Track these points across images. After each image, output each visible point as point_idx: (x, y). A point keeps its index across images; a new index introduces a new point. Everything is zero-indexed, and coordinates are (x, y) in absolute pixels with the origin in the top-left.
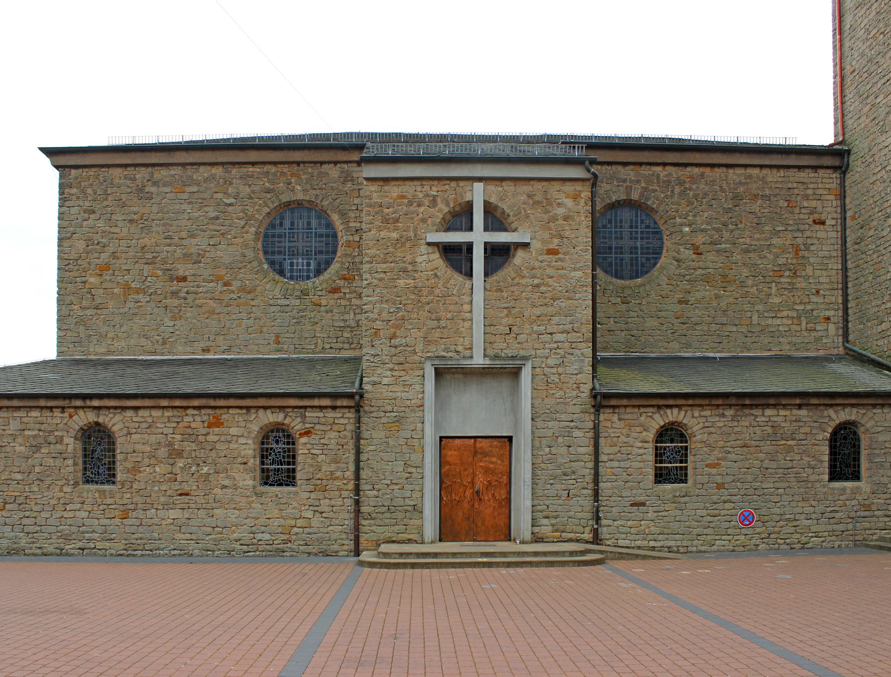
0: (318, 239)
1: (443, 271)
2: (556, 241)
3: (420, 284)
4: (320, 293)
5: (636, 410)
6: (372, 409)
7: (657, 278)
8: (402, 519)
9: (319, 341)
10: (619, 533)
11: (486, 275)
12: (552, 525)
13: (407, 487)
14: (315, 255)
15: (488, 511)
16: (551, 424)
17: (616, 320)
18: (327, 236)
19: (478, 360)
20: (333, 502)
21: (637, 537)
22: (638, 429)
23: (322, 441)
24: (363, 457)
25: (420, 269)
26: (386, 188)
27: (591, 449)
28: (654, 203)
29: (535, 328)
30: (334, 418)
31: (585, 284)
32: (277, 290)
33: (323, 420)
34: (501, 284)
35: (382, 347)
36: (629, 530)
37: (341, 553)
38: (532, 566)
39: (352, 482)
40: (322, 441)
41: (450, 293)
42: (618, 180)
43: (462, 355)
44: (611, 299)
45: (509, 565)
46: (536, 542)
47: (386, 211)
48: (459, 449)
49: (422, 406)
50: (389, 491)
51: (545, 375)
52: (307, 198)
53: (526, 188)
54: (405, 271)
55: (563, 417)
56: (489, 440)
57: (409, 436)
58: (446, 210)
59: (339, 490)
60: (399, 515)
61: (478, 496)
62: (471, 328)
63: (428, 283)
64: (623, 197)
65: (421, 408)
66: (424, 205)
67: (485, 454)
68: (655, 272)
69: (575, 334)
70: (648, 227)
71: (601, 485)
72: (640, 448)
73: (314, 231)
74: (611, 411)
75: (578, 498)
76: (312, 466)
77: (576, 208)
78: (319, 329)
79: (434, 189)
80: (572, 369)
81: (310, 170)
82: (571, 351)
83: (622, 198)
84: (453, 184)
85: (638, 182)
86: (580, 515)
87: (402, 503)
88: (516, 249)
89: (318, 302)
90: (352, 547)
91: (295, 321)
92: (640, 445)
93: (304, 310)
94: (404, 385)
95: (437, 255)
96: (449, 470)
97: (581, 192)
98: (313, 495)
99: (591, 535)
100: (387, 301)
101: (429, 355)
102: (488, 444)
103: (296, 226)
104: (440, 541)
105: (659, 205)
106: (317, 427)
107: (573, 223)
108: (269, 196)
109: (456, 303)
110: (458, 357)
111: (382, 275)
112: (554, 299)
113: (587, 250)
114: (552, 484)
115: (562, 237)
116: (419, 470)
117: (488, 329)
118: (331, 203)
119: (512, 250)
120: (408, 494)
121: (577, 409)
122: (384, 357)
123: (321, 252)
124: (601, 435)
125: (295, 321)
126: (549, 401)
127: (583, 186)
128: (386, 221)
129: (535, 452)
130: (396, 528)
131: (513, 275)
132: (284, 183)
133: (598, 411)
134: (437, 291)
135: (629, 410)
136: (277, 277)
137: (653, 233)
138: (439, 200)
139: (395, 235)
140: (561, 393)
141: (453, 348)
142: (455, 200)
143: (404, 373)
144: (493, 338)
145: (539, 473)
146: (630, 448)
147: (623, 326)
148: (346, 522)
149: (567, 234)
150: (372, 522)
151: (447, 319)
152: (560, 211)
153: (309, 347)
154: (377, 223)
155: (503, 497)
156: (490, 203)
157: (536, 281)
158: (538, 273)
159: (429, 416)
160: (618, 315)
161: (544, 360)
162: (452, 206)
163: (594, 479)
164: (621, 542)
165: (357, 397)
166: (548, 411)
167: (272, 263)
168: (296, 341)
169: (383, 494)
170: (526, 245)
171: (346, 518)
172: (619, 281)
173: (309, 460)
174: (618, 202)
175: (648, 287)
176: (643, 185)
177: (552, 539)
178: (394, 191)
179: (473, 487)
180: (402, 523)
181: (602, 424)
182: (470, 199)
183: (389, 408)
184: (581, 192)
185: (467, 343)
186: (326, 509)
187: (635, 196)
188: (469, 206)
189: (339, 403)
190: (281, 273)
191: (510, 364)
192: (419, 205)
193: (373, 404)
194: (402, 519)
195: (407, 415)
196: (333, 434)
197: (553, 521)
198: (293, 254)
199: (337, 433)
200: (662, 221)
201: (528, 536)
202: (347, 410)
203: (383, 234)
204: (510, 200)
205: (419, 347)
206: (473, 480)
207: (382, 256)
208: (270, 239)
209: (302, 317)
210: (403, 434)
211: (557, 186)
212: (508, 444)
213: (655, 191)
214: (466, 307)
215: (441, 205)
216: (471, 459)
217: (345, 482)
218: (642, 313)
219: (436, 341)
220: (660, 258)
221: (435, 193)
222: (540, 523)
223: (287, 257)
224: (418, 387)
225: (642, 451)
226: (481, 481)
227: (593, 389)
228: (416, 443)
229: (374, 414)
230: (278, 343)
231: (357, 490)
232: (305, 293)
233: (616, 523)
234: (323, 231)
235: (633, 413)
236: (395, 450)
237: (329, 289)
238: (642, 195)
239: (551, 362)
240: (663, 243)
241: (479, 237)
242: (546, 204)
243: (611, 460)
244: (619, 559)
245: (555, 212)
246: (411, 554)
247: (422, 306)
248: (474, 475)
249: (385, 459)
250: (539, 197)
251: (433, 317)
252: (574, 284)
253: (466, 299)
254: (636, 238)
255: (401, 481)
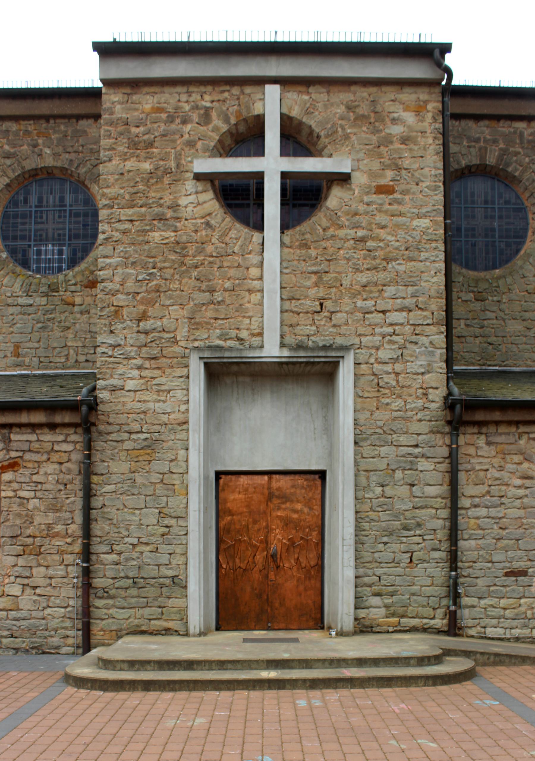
0: (73, 219)
1: (219, 218)
2: (390, 174)
3: (184, 238)
4: (73, 288)
5: (513, 429)
6: (110, 428)
7: (521, 267)
8: (155, 598)
9: (72, 352)
10: (488, 617)
11: (285, 227)
12: (387, 606)
13: (163, 548)
14: (70, 239)
15: (290, 585)
16: (384, 450)
17: (468, 322)
18: (86, 215)
19: (272, 350)
20: (51, 572)
21: (515, 623)
22: (517, 458)
23: (35, 478)
24: (96, 502)
25: (184, 215)
26: (135, 97)
27: (445, 489)
28: (516, 170)
29: (359, 303)
30: (53, 443)
31: (434, 237)
32: (17, 285)
33: (36, 445)
34: (308, 236)
35: (126, 334)
36: (502, 612)
37: (64, 650)
38: (353, 686)
39: (80, 541)
40: (35, 478)
41: (230, 251)
42: (469, 139)
43: (247, 344)
44: (461, 294)
45: (314, 684)
46: (362, 632)
47: (134, 130)
48: (246, 490)
49: (186, 423)
50: (135, 555)
51: (374, 374)
52: (59, 164)
53: (344, 96)
54: (161, 218)
55: (403, 439)
56: (292, 477)
57: (166, 470)
58: (224, 128)
59: (60, 552)
60: (151, 592)
61: (275, 561)
62: (261, 304)
63: (196, 237)
64: (476, 161)
65: (184, 427)
66: (191, 121)
67: (285, 498)
68: (518, 261)
69: (420, 312)
70: (507, 202)
71: (461, 543)
72: (519, 487)
73: (68, 208)
74: (475, 430)
75: (425, 565)
76: (19, 515)
77: (421, 126)
78: (71, 336)
79: (207, 97)
80: (415, 366)
81: (62, 127)
82: (414, 338)
83: (474, 162)
84: (236, 90)
85: (495, 141)
86: (428, 591)
87: (155, 573)
88: (329, 188)
89: (70, 300)
90: (80, 640)
91: (40, 325)
92: (519, 482)
93: (52, 311)
94: (158, 391)
95: (210, 195)
96: (230, 523)
97: (426, 102)
98: (21, 561)
99: (445, 621)
100: (133, 263)
101: (196, 344)
102: (290, 483)
103: (45, 203)
104: (218, 629)
105: (523, 172)
106: (27, 456)
107: (416, 148)
108: (8, 162)
109: (239, 266)
110: (241, 347)
111: (128, 226)
112: (387, 260)
113: (436, 188)
114: (385, 543)
115: (399, 169)
116: (181, 522)
117: (287, 305)
118: (90, 170)
119: (325, 190)
120: (164, 559)
121: (424, 427)
122: (129, 349)
123: (77, 236)
124: (460, 467)
125: (40, 325)
126: (382, 416)
127: (430, 93)
128: (134, 144)
129: (360, 494)
130: (147, 612)
131: (325, 223)
132: (29, 145)
133: (457, 429)
134: (210, 248)
135: (502, 429)
136: (19, 269)
137: (515, 210)
138: (214, 114)
139: (147, 166)
140: (399, 403)
141: (233, 333)
142: (238, 113)
143: (159, 372)
144: (294, 319)
145: (366, 526)
146: (504, 488)
147: (478, 331)
148: (72, 602)
149: (406, 163)
150: (111, 602)
151: (225, 290)
152: (396, 130)
153: (58, 360)
154: (121, 148)
155: (313, 563)
156: (290, 119)
157: (360, 233)
158: (364, 220)
159: (196, 438)
160: (470, 315)
161: (373, 351)
162: (233, 121)
163: (450, 535)
164: (490, 632)
165: (84, 408)
166: (379, 431)
167: (13, 252)
168: (41, 352)
169: (127, 560)
170: (344, 179)
171: (69, 595)
172: (471, 273)
173: (15, 508)
174: (469, 168)
175: (509, 280)
176: (502, 146)
177: (385, 628)
178: (147, 101)
179: (267, 548)
180: (157, 604)
181: (462, 450)
182: (261, 112)
183: (136, 427)
184: (426, 102)
185: (254, 326)
186: (41, 582)
187: (491, 160)
188: (259, 123)
189: (58, 419)
190: (25, 264)
191: (321, 356)
192: (184, 122)
193: (111, 420)
194: (155, 598)
195: (163, 437)
196: (51, 468)
197: (388, 600)
198: (41, 239)
199: (57, 466)
200: (527, 194)
201: (348, 624)
202: (72, 431)
203: (130, 164)
204: (322, 111)
205: (182, 333)
206: (266, 537)
207: (127, 197)
208: (11, 221)
209: (49, 320)
210: (156, 466)
211: (390, 93)
212: (319, 482)
213: (517, 154)
214: (254, 272)
215: (217, 121)
216: (262, 507)
217: (69, 540)
218: (502, 314)
219: (208, 323)
220: (524, 243)
221: (208, 105)
222: (367, 604)
223: (32, 243)
224: (179, 394)
225: (521, 492)
226: (278, 538)
227: (450, 394)
228: (176, 480)
229: (114, 436)
230: (18, 355)
231: (87, 553)
232: (53, 288)
233: (483, 602)
234: (81, 208)
235: (508, 434)
236: (144, 491)
237: (85, 282)
238: (500, 158)
239: (383, 354)
240: (528, 224)
241: (272, 164)
242: (375, 119)
243: (476, 506)
244: (494, 664)
245: (387, 131)
246: (148, 662)
247: (187, 271)
248: (268, 530)
249: (130, 504)
250: (364, 109)
251: (204, 288)
252: (418, 238)
253: (254, 259)
254: (492, 217)
255: (153, 539)
